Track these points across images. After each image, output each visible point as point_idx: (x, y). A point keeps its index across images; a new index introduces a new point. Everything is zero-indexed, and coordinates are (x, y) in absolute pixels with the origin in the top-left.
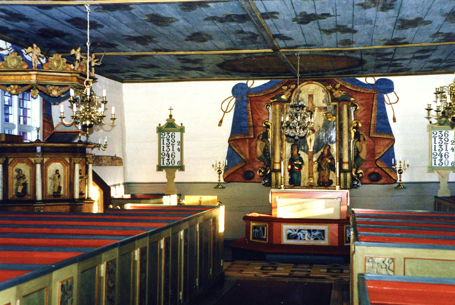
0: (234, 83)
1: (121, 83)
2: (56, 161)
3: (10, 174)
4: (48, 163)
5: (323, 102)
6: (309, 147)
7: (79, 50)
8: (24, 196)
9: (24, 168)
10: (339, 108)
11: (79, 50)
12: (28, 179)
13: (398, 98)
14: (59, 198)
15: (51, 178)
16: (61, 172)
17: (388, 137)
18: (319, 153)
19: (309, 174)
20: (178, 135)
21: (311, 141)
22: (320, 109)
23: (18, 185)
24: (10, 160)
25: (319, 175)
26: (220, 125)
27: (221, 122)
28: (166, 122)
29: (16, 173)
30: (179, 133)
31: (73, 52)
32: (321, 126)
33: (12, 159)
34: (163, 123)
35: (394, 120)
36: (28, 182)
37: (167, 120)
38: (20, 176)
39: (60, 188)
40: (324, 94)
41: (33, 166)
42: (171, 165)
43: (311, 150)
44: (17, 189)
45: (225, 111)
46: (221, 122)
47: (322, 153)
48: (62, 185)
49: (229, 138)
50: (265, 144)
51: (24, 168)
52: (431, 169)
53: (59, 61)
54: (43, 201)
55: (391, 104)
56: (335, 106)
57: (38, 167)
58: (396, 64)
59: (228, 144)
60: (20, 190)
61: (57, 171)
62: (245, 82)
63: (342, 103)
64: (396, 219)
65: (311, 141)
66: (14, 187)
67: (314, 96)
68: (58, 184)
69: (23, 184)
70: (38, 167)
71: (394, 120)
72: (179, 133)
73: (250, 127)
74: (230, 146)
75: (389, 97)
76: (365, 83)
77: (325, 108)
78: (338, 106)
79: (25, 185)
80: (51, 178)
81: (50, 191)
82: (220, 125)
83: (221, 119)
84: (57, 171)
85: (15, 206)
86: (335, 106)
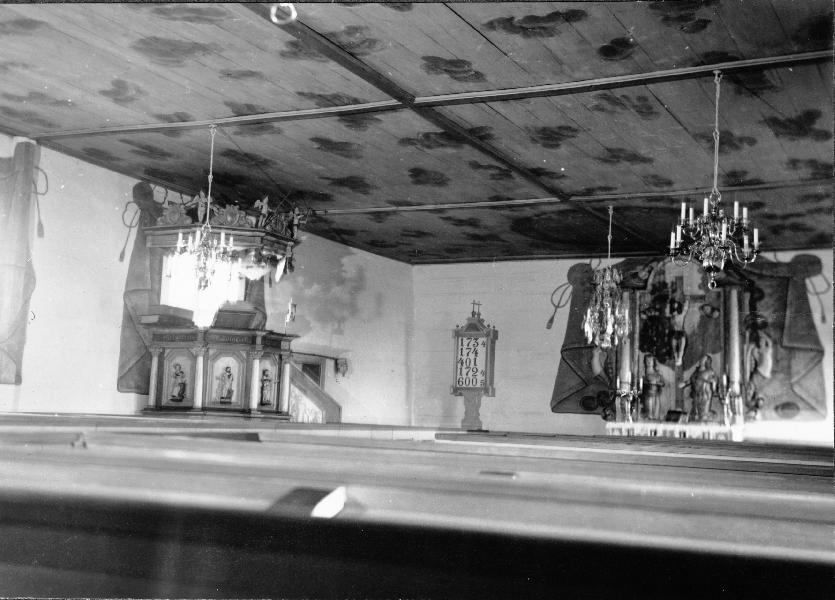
0: (567, 264)
1: (410, 266)
2: (227, 353)
3: (166, 371)
4: (216, 357)
5: (700, 287)
7: (266, 200)
9: (182, 361)
10: (725, 296)
11: (266, 200)
14: (227, 407)
15: (217, 378)
16: (235, 371)
17: (813, 347)
18: (693, 369)
19: (677, 401)
22: (695, 298)
24: (167, 351)
25: (693, 403)
26: (549, 327)
27: (551, 321)
28: (466, 322)
29: (174, 370)
31: (258, 203)
32: (696, 326)
34: (463, 323)
37: (469, 319)
38: (179, 374)
39: (230, 392)
40: (701, 276)
41: (194, 358)
42: (471, 385)
46: (551, 321)
47: (698, 368)
48: (234, 388)
51: (182, 361)
52: (359, 284)
53: (233, 215)
54: (204, 409)
55: (817, 294)
56: (719, 293)
57: (200, 360)
58: (320, 105)
59: (560, 356)
61: (227, 369)
62: (587, 261)
63: (728, 289)
67: (685, 279)
68: (228, 386)
70: (200, 360)
77: (702, 298)
78: (722, 294)
80: (217, 378)
81: (215, 396)
82: (549, 327)
83: (549, 318)
84: (227, 369)
86: (719, 294)
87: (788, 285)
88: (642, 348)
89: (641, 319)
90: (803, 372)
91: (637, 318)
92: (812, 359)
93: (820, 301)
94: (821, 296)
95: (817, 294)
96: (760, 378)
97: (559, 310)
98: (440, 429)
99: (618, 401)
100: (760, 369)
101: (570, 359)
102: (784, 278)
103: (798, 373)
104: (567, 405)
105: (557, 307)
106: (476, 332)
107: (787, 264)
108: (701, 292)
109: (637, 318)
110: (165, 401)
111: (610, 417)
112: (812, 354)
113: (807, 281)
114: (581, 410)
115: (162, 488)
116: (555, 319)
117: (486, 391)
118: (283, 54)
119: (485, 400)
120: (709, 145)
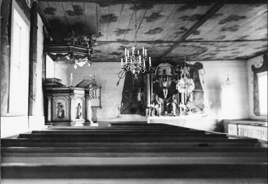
6: (165, 96)
8: (62, 118)
12: (64, 109)
13: (205, 72)
20: (98, 90)
21: (165, 92)
22: (170, 76)
23: (58, 112)
27: (118, 83)
30: (99, 89)
33: (55, 97)
35: (203, 82)
36: (65, 110)
43: (166, 97)
44: (58, 114)
45: (120, 77)
46: (118, 83)
49: (123, 92)
50: (142, 94)
55: (202, 75)
60: (60, 114)
61: (79, 104)
64: (64, 142)
65: (165, 92)
66: (57, 113)
69: (62, 111)
71: (203, 82)
72: (99, 89)
73: (133, 86)
74: (123, 95)
75: (201, 71)
76: (189, 64)
79: (63, 111)
83: (118, 82)
85: (58, 124)
87: (193, 71)
88: (153, 93)
89: (153, 83)
90: (198, 99)
91: (152, 83)
92: (201, 94)
93: (203, 77)
94: (203, 75)
95: (202, 75)
96: (189, 102)
97: (121, 79)
98: (261, 134)
99: (147, 110)
100: (189, 99)
101: (125, 96)
102: (192, 69)
103: (197, 99)
104: (126, 111)
105: (120, 78)
106: (96, 87)
107: (193, 65)
108: (171, 75)
109: (152, 83)
110: (54, 118)
111: (143, 115)
112: (201, 93)
113: (199, 71)
114: (131, 113)
115: (27, 149)
116: (119, 82)
117: (100, 107)
118: (200, 31)
119: (98, 110)
120: (217, 38)
